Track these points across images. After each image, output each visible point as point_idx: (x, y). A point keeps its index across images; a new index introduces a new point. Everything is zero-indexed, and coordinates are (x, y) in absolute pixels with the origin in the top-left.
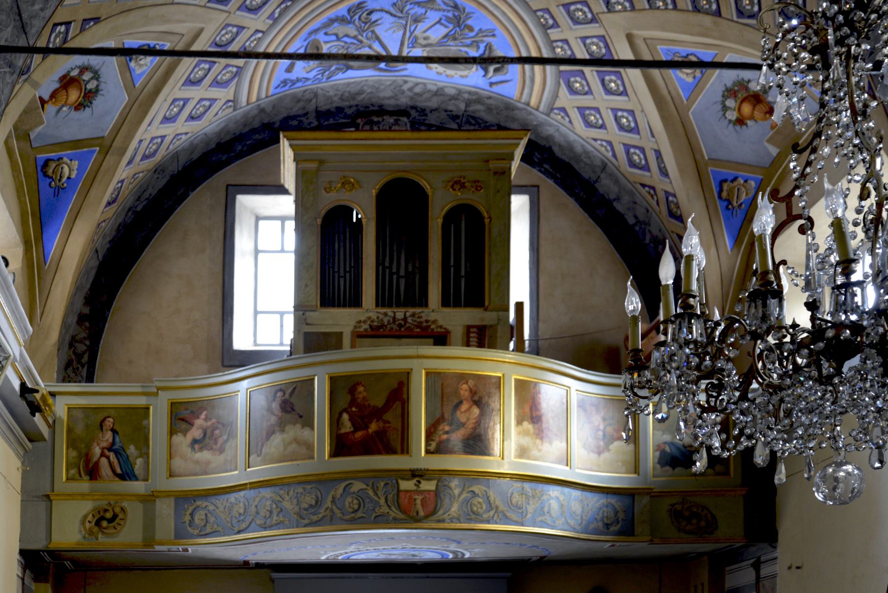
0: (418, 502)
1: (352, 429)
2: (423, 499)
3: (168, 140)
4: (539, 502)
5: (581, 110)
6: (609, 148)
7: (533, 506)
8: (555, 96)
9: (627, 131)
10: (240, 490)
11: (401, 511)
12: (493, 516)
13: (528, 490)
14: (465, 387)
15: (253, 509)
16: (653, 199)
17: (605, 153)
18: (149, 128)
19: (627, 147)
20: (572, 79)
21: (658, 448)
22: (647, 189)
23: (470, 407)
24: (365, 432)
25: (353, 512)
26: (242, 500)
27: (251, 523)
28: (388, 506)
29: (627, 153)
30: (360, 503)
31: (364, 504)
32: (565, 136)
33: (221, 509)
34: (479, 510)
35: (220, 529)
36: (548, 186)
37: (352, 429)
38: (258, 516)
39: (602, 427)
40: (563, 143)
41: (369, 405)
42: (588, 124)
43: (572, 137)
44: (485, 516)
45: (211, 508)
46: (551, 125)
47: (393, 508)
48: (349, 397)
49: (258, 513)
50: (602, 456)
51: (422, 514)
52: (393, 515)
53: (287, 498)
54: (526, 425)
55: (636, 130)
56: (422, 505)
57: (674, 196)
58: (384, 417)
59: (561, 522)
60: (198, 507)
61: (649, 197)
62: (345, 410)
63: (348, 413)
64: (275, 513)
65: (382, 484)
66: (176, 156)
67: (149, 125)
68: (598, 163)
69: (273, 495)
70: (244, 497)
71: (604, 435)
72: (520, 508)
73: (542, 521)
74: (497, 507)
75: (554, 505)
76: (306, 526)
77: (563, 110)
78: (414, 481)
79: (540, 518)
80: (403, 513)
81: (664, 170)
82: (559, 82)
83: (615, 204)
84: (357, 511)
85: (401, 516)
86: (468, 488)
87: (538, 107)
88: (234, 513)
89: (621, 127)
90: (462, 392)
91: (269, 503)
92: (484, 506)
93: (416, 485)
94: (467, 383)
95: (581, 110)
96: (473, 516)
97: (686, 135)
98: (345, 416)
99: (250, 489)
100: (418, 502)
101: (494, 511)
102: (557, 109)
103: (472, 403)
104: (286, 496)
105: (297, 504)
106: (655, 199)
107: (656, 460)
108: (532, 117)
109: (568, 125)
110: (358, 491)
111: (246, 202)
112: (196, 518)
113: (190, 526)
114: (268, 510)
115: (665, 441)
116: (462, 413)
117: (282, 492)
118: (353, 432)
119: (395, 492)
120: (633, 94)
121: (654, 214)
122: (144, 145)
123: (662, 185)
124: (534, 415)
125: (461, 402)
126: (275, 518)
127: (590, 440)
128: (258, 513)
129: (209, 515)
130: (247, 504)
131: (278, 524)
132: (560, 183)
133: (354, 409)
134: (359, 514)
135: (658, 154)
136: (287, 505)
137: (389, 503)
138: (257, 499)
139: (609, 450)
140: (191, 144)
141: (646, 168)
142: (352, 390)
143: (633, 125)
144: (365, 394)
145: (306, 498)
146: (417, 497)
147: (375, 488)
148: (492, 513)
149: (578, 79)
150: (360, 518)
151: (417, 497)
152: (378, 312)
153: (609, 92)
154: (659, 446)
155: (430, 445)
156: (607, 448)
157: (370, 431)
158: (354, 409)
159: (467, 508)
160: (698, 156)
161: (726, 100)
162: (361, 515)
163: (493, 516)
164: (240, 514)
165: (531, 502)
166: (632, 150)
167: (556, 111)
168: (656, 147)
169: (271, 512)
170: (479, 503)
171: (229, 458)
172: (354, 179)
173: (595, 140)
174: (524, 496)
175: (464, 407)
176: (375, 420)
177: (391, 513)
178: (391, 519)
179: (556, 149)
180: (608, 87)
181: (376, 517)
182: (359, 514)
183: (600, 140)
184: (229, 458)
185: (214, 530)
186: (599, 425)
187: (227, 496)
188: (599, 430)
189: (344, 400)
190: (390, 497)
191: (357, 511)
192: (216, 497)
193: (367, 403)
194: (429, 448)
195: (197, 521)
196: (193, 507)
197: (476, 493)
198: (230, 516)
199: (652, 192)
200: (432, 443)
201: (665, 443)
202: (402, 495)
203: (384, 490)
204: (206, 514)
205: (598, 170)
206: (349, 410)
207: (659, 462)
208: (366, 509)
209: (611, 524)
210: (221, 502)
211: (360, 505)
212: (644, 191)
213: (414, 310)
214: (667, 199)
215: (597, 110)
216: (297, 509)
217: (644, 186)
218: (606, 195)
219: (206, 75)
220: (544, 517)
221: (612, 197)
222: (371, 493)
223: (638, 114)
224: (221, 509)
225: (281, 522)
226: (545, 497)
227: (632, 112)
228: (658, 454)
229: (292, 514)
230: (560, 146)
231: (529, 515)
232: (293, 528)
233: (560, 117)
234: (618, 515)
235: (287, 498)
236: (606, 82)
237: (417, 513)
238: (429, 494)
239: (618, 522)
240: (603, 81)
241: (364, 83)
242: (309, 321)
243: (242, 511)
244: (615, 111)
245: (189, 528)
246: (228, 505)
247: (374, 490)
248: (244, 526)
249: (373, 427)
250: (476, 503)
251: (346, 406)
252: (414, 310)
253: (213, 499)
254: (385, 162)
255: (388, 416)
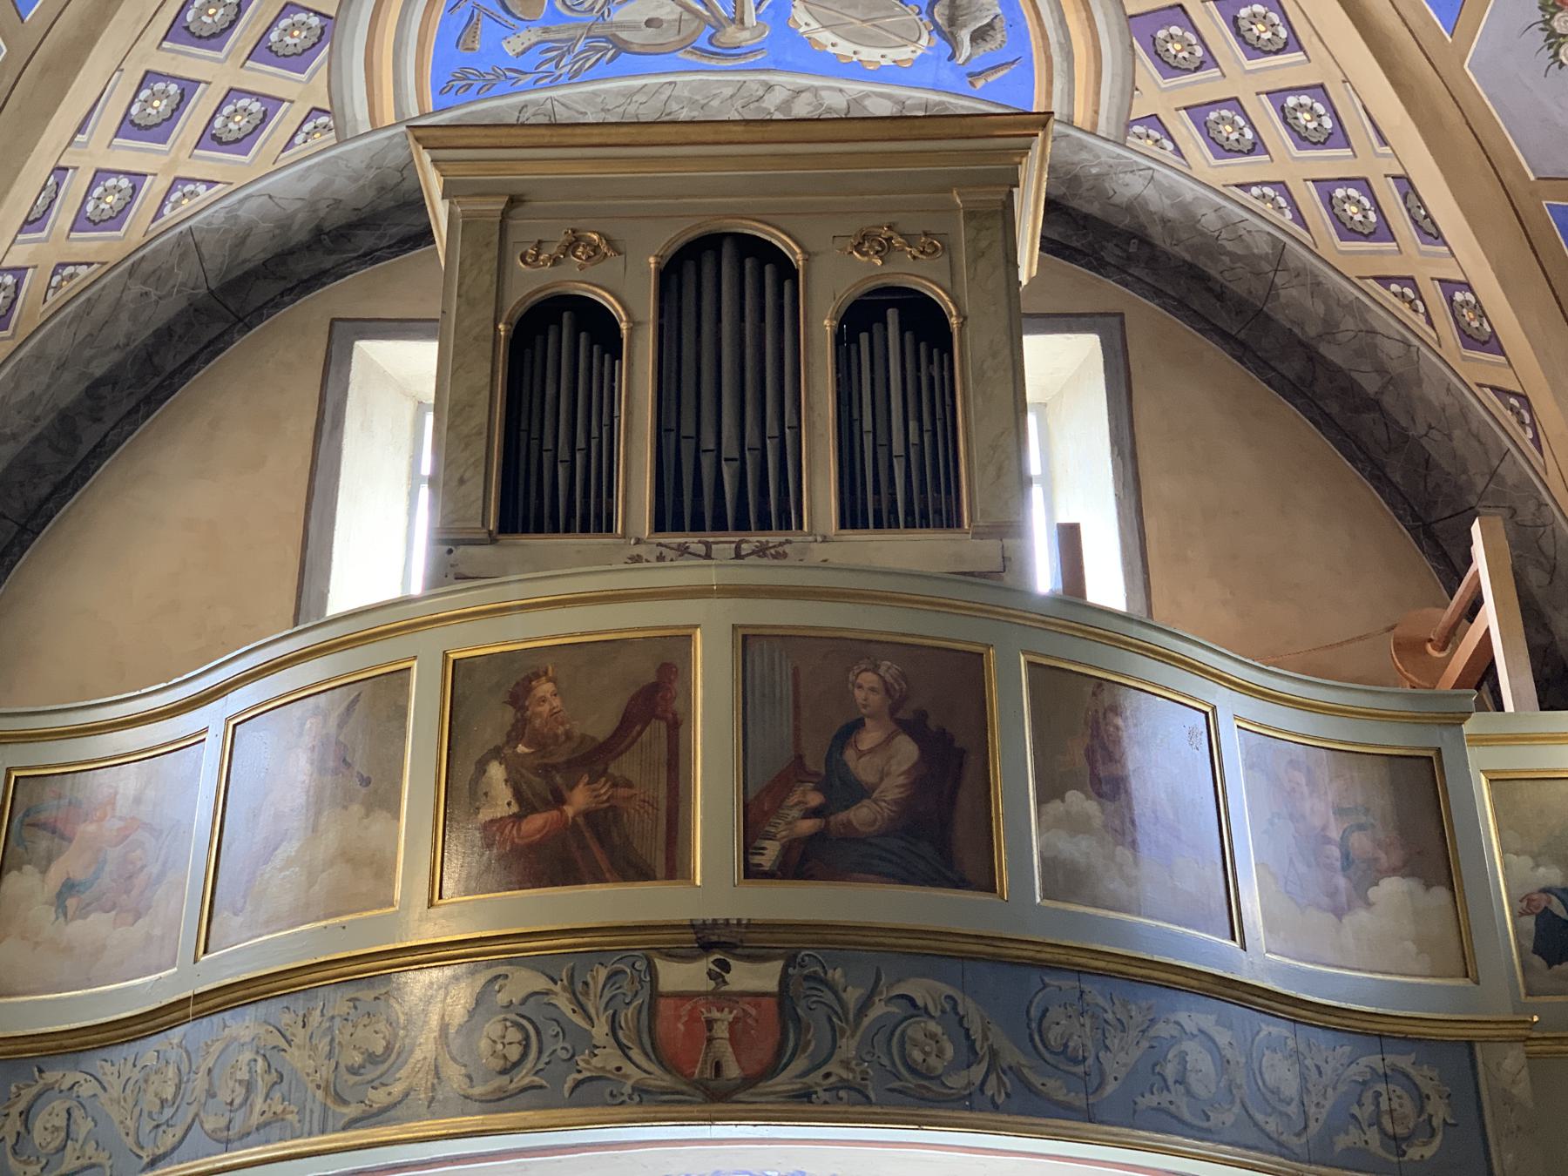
0: (721, 1031)
1: (515, 809)
2: (736, 1019)
3: (153, 189)
4: (1145, 1044)
5: (1197, 112)
6: (1282, 201)
7: (1122, 1057)
8: (1130, 88)
9: (1316, 144)
10: (172, 1025)
11: (661, 1063)
12: (983, 1083)
13: (1101, 1001)
14: (868, 679)
15: (200, 1083)
16: (1416, 311)
17: (1275, 216)
18: (79, 138)
19: (1325, 186)
20: (1161, 34)
21: (1525, 905)
22: (1394, 287)
23: (889, 740)
24: (555, 813)
25: (504, 1072)
26: (173, 1056)
27: (189, 1128)
28: (623, 1048)
29: (1329, 201)
30: (527, 1038)
31: (540, 1041)
32: (1172, 193)
33: (115, 1091)
34: (932, 1060)
35: (101, 1157)
36: (1144, 314)
37: (515, 809)
38: (211, 1101)
39: (1335, 834)
40: (1171, 214)
41: (568, 736)
42: (1222, 149)
43: (1189, 191)
44: (956, 1081)
45: (87, 1089)
46: (1133, 169)
47: (635, 1054)
48: (509, 715)
49: (211, 1094)
50: (1346, 920)
51: (733, 1071)
52: (637, 1075)
53: (300, 1036)
54: (1077, 801)
55: (1338, 137)
56: (733, 1040)
57: (1467, 286)
58: (612, 769)
59: (1229, 1119)
60: (49, 1088)
61: (1405, 307)
62: (496, 753)
63: (503, 761)
64: (261, 1087)
65: (603, 974)
66: (189, 244)
67: (81, 129)
68: (1263, 247)
69: (262, 1031)
70: (180, 1045)
71: (1346, 857)
72: (1076, 1061)
73: (1159, 1109)
74: (994, 1053)
75: (1200, 1060)
76: (351, 1124)
77: (1154, 120)
78: (706, 964)
79: (1151, 1100)
80: (667, 1070)
81: (1426, 224)
82: (1132, 45)
83: (1323, 349)
84: (516, 1064)
85: (660, 1078)
86: (890, 986)
87: (1095, 124)
88: (149, 1101)
89: (1303, 139)
90: (859, 695)
91: (247, 1055)
92: (949, 1051)
93: (710, 974)
94: (875, 669)
95: (1197, 112)
96: (911, 1082)
97: (1468, 123)
98: (496, 771)
99: (199, 1016)
100: (721, 1031)
101: (984, 1065)
102: (1138, 121)
103: (892, 727)
104: (300, 1032)
105: (330, 1055)
106: (1421, 309)
107: (1529, 944)
108: (1084, 155)
109: (1173, 160)
110: (524, 1002)
111: (371, 353)
112: (38, 1125)
113: (15, 1153)
114: (240, 1082)
115: (1543, 884)
116: (861, 754)
117: (287, 1018)
118: (517, 818)
119: (644, 996)
120: (1315, 39)
121: (1423, 349)
122: (75, 185)
123: (1427, 266)
124: (1102, 771)
125: (857, 725)
126: (259, 1104)
127: (1302, 868)
128: (211, 1094)
129: (77, 1114)
130: (185, 1067)
131: (266, 1124)
132: (1180, 307)
133: (521, 749)
134: (523, 1077)
135: (1405, 183)
136: (297, 1059)
137: (620, 1034)
138: (216, 1048)
139: (1369, 904)
140: (232, 215)
141: (1383, 232)
142: (519, 697)
143: (1328, 123)
144: (556, 702)
145: (360, 1032)
146: (716, 1014)
147: (579, 987)
148: (978, 1072)
149: (1175, 30)
150: (524, 1090)
151: (716, 1014)
152: (659, 545)
153: (1254, 49)
154: (1528, 899)
155: (760, 851)
156: (1361, 895)
157: (570, 811)
158: (521, 749)
159: (890, 1053)
160: (1508, 176)
161: (1553, 15)
162: (526, 1081)
163: (983, 1083)
164: (163, 1102)
165: (1114, 1042)
166: (1339, 193)
167: (1137, 129)
168: (1399, 171)
169: (249, 1086)
170: (932, 1036)
171: (157, 932)
172: (599, 234)
173: (1244, 187)
174: (1087, 1021)
175: (869, 738)
176: (586, 779)
177: (629, 1068)
178: (627, 1089)
179: (1156, 233)
180: (1248, 35)
181: (578, 1084)
182: (523, 1077)
183: (1256, 184)
184: (157, 932)
185: (84, 1162)
186: (1325, 828)
187: (137, 1046)
188: (1328, 841)
189: (494, 723)
190: (627, 1015)
191: (516, 1064)
192: (104, 1053)
193: (561, 730)
194: (756, 860)
195: (38, 1135)
196: (35, 1090)
197: (920, 1002)
198: (137, 1111)
199: (1408, 291)
200: (767, 843)
201: (1546, 891)
202: (662, 1003)
203: (607, 995)
204: (69, 1112)
205: (1266, 267)
206: (507, 751)
207: (1537, 950)
208: (545, 1058)
209: (1407, 1139)
210: (116, 1065)
211: (527, 1047)
212: (1386, 295)
213: (763, 539)
214: (1451, 301)
215: (1235, 103)
216: (326, 1072)
217: (1384, 281)
218: (1296, 330)
219: (233, 24)
220: (1166, 1097)
221: (1312, 331)
222: (563, 1003)
223: (1336, 91)
224: (115, 1091)
225: (278, 1118)
226: (1163, 1030)
227: (1319, 90)
228: (1530, 922)
229: (311, 1086)
230: (1165, 221)
231: (1111, 1087)
232: (310, 1134)
233: (1150, 142)
234: (1430, 1109)
235: (300, 1036)
236: (1244, 24)
237: (718, 1067)
238: (757, 1006)
239: (1433, 1134)
240: (1234, 23)
241: (667, 92)
242: (464, 570)
243: (169, 1092)
244: (1278, 95)
245: (11, 1161)
246: (136, 1075)
247: (574, 993)
248: (169, 1140)
249: (579, 799)
250: (920, 1036)
251: (499, 740)
252: (763, 539)
253: (95, 1061)
254: (683, 197)
255: (626, 766)
